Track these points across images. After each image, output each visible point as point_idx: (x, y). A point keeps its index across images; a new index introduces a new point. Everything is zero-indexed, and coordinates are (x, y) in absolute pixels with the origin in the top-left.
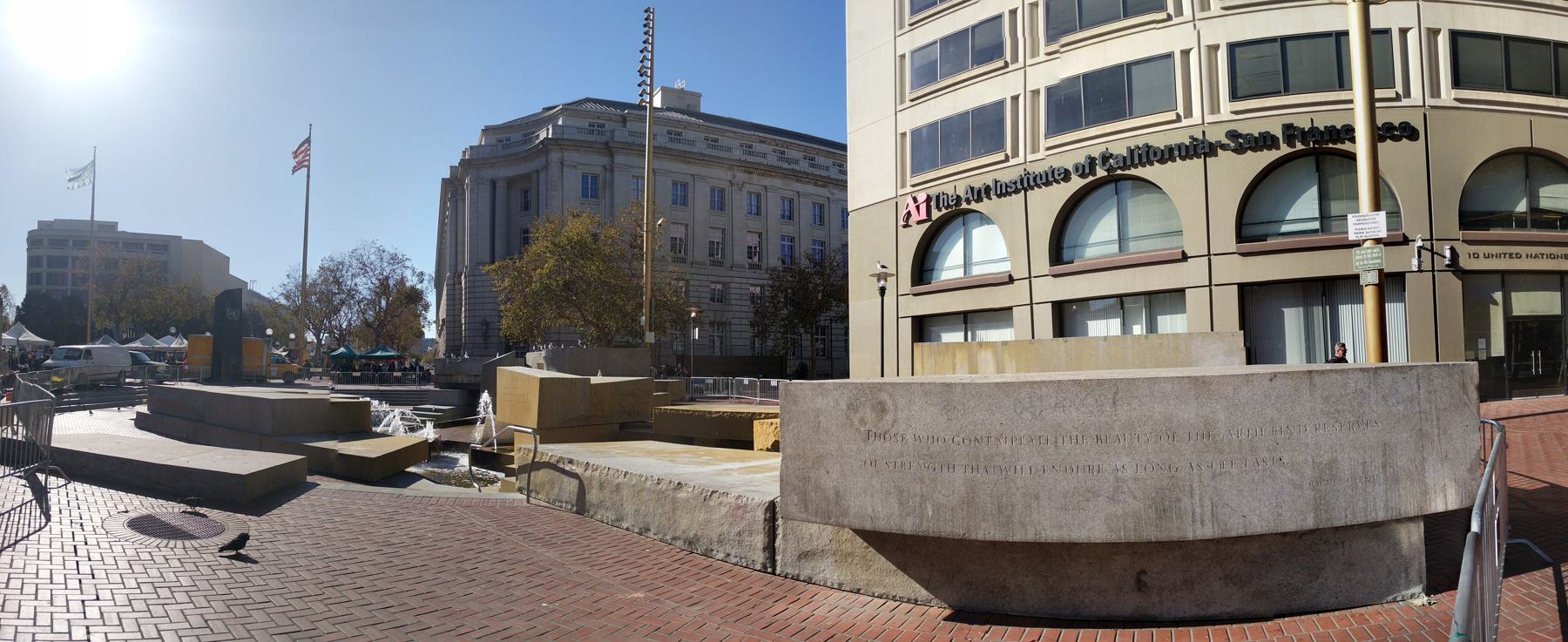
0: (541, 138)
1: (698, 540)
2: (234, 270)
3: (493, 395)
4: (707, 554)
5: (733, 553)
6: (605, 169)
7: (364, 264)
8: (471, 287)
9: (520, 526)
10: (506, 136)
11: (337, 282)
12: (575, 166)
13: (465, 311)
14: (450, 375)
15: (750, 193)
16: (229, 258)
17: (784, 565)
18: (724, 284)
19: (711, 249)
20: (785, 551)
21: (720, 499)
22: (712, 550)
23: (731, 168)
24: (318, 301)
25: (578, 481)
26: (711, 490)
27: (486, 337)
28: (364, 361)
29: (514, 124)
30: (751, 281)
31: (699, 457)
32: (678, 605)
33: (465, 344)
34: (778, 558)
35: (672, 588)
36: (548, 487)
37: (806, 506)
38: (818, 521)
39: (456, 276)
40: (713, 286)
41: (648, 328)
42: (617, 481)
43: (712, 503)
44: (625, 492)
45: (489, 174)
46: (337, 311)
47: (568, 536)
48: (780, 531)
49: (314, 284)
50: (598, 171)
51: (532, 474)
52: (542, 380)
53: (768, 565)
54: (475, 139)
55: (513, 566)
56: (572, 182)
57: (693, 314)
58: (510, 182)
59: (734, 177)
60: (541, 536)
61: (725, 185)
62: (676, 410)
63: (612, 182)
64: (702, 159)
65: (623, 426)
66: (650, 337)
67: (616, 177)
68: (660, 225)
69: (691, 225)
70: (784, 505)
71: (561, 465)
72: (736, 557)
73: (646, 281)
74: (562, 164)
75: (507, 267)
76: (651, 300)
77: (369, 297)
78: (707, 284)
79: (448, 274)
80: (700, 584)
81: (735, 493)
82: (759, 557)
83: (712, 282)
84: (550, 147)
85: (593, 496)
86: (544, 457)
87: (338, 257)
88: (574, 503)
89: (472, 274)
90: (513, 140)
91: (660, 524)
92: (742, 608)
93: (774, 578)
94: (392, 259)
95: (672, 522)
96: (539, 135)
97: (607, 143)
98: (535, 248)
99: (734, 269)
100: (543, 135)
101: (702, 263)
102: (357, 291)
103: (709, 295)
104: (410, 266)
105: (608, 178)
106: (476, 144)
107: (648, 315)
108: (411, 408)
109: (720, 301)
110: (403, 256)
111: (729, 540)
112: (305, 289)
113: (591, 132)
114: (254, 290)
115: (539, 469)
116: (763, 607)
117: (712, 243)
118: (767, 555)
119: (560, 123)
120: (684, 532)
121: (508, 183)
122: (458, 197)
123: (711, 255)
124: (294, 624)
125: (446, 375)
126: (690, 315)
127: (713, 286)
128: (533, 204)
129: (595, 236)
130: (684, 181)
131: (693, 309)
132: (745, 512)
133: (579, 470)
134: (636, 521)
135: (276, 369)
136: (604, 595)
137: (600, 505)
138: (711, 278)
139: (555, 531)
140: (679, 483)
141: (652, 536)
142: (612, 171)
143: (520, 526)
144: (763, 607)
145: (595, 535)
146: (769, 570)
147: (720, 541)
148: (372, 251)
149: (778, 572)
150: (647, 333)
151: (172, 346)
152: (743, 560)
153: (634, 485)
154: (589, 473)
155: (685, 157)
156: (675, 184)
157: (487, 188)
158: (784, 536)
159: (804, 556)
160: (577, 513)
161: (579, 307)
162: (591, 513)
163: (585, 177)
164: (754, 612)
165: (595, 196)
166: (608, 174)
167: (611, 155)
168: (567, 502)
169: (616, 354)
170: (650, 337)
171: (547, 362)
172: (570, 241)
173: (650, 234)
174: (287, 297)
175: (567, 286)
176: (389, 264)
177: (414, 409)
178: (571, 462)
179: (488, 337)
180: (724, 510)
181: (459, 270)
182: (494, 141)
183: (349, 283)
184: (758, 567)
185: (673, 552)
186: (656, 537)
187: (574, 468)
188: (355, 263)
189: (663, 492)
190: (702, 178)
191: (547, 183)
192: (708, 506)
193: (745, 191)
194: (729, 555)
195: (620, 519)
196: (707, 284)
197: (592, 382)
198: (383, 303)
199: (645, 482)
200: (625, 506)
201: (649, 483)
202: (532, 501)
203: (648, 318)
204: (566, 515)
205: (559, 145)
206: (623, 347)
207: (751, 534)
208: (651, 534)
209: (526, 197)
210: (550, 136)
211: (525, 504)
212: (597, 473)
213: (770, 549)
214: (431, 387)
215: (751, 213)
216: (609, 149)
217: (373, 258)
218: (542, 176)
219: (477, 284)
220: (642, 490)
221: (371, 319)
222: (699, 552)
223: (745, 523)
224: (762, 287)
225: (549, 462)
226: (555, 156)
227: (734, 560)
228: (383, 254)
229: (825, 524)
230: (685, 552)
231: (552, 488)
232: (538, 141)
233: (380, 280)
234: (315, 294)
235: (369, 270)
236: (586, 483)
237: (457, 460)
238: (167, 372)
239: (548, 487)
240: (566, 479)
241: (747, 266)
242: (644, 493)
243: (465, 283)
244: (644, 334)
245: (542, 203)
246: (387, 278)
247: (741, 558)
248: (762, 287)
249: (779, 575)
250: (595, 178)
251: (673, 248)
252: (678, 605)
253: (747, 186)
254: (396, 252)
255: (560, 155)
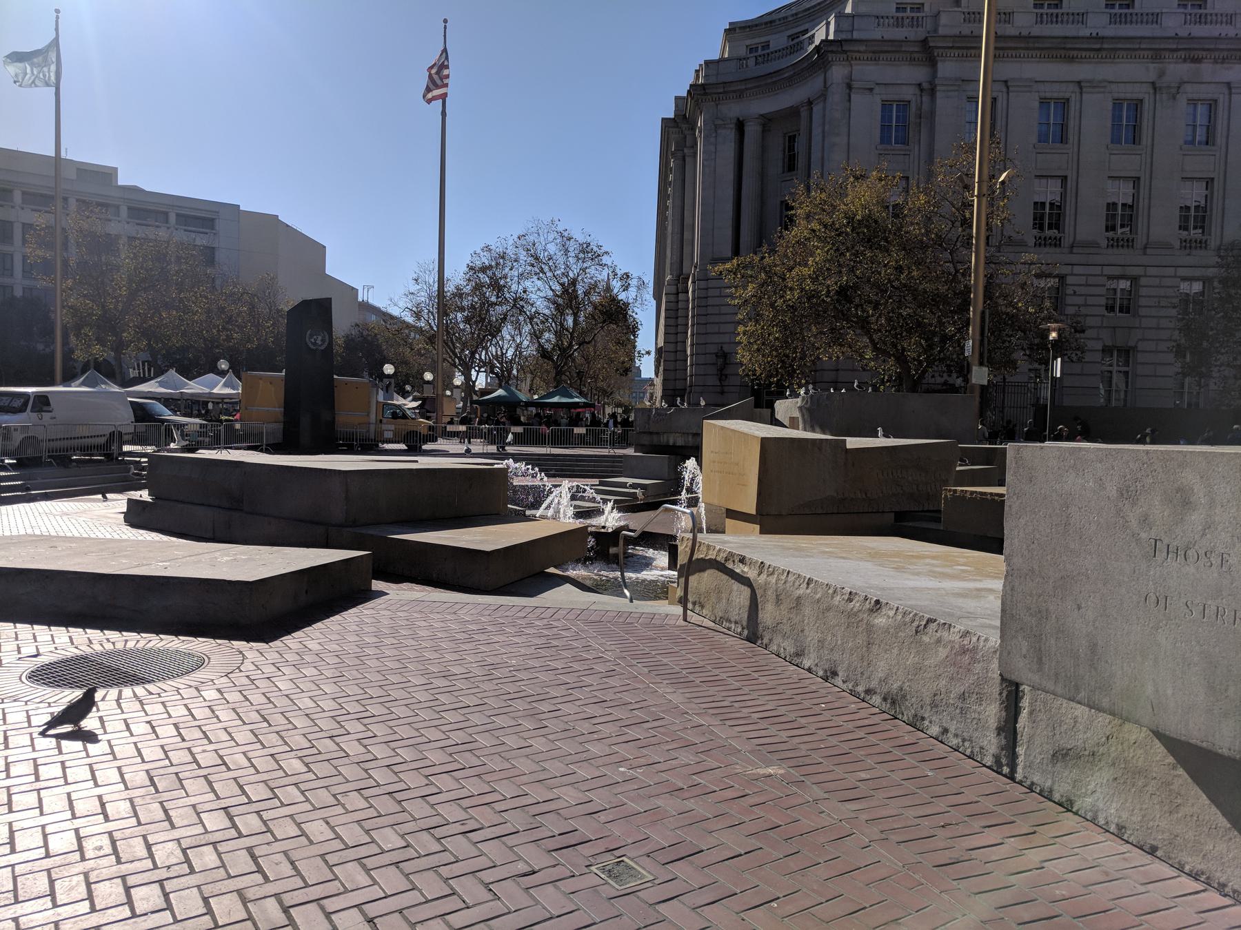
0: (817, 42)
1: (904, 697)
2: (335, 268)
3: (699, 462)
4: (916, 723)
5: (952, 729)
6: (922, 91)
7: (537, 258)
8: (702, 300)
9: (653, 653)
10: (763, 39)
11: (497, 286)
12: (871, 90)
13: (692, 335)
14: (657, 433)
15: (1193, 102)
16: (325, 247)
17: (1029, 766)
18: (1134, 280)
19: (1111, 217)
20: (1031, 738)
21: (938, 635)
22: (923, 719)
23: (1157, 55)
24: (467, 320)
25: (749, 590)
26: (927, 616)
27: (722, 375)
28: (533, 410)
29: (774, 17)
30: (1182, 272)
31: (951, 566)
32: (826, 796)
33: (691, 386)
34: (1020, 750)
35: (834, 768)
36: (713, 599)
37: (1040, 661)
38: (1059, 690)
39: (680, 279)
40: (1112, 284)
41: (977, 362)
42: (801, 592)
43: (926, 639)
44: (807, 610)
45: (733, 110)
46: (495, 331)
47: (716, 672)
48: (1025, 703)
49: (459, 294)
50: (909, 93)
51: (692, 578)
52: (765, 442)
53: (1004, 761)
54: (714, 48)
55: (610, 711)
56: (866, 111)
57: (1053, 335)
58: (767, 122)
59: (1162, 74)
60: (677, 669)
61: (1142, 92)
62: (981, 493)
63: (932, 113)
64: (1099, 48)
65: (900, 516)
66: (980, 376)
67: (939, 102)
68: (1003, 182)
69: (1070, 183)
70: (1005, 654)
71: (730, 565)
72: (956, 736)
73: (976, 281)
74: (849, 87)
75: (750, 265)
76: (983, 313)
77: (547, 312)
78: (1102, 280)
79: (669, 278)
80: (881, 770)
81: (960, 627)
82: (991, 743)
83: (1110, 278)
84: (830, 57)
85: (768, 614)
86: (711, 552)
87: (498, 248)
88: (745, 624)
89: (704, 277)
90: (773, 47)
91: (849, 665)
92: (926, 822)
93: (1010, 785)
94: (583, 251)
95: (865, 663)
96: (813, 36)
97: (924, 42)
98: (799, 231)
99: (1148, 251)
100: (820, 35)
101: (1094, 245)
102: (527, 302)
103: (1103, 301)
104: (610, 264)
105: (925, 107)
106: (716, 57)
107: (978, 337)
108: (596, 481)
109: (1125, 309)
110: (600, 247)
111: (947, 705)
112: (443, 302)
113: (899, 23)
114: (371, 301)
115: (703, 570)
116: (961, 830)
117: (1112, 206)
118: (1004, 742)
119: (848, 10)
120: (884, 681)
121: (764, 125)
122: (686, 151)
123: (1110, 228)
124: (398, 755)
125: (651, 433)
126: (1047, 337)
127: (1112, 284)
128: (801, 162)
129: (897, 211)
130: (1061, 95)
131: (1053, 325)
132: (974, 660)
133: (750, 573)
134: (820, 658)
135: (392, 427)
136: (716, 764)
137: (775, 629)
138: (1108, 271)
139: (701, 664)
140: (877, 602)
141: (840, 683)
142: (932, 91)
143: (653, 653)
144: (961, 830)
145: (756, 675)
146: (1006, 770)
147: (934, 705)
148: (551, 237)
149: (1019, 776)
150: (975, 369)
151: (215, 391)
152: (967, 744)
153: (818, 601)
154: (763, 576)
155: (1064, 50)
156: (1044, 102)
157: (730, 134)
158: (1031, 713)
159: (1061, 756)
160: (748, 639)
161: (864, 325)
162: (766, 641)
163: (886, 106)
164: (941, 833)
165: (904, 141)
166: (926, 99)
167: (932, 62)
168: (736, 623)
169: (916, 403)
170: (980, 376)
171: (803, 416)
172: (851, 219)
173: (984, 200)
174: (418, 315)
175: (844, 293)
176: (578, 259)
177: (601, 484)
178: (742, 560)
179: (726, 376)
180: (943, 652)
181: (685, 270)
182: (742, 52)
183: (514, 287)
184: (989, 760)
185: (863, 714)
186: (844, 687)
187: (746, 569)
188: (523, 256)
189: (856, 614)
190: (1096, 85)
191: (824, 124)
192: (920, 643)
193: (1182, 100)
194: (946, 731)
195: (799, 654)
196: (1102, 280)
197: (848, 446)
198: (570, 321)
199: (832, 597)
200: (806, 632)
201: (838, 598)
202: (693, 617)
203: (977, 343)
204: (731, 641)
205: (845, 52)
206: (939, 391)
207: (980, 700)
208: (838, 681)
209: (791, 148)
210: (831, 37)
211: (681, 622)
212: (773, 579)
213: (1009, 730)
214: (630, 451)
215: (1192, 142)
216: (927, 53)
217: (552, 248)
218: (817, 109)
219: (711, 293)
220: (828, 609)
221: (548, 347)
222: (905, 718)
223: (972, 679)
224: (1206, 281)
225: (715, 560)
226: (838, 72)
227: (954, 742)
228: (568, 243)
229: (1070, 699)
230: (887, 716)
231: (719, 599)
232: (812, 47)
233: (562, 285)
234: (462, 309)
235: (546, 269)
236: (759, 593)
237: (653, 559)
238: (201, 434)
239: (713, 599)
240: (736, 586)
241: (1177, 244)
242: (831, 614)
243: (693, 291)
244: (969, 370)
245: (816, 156)
246: (574, 282)
247: (963, 741)
248: (1206, 281)
249: (1020, 783)
250: (904, 105)
251: (1038, 223)
252: (826, 796)
253: (1188, 88)
254: (589, 239)
255: (846, 71)
